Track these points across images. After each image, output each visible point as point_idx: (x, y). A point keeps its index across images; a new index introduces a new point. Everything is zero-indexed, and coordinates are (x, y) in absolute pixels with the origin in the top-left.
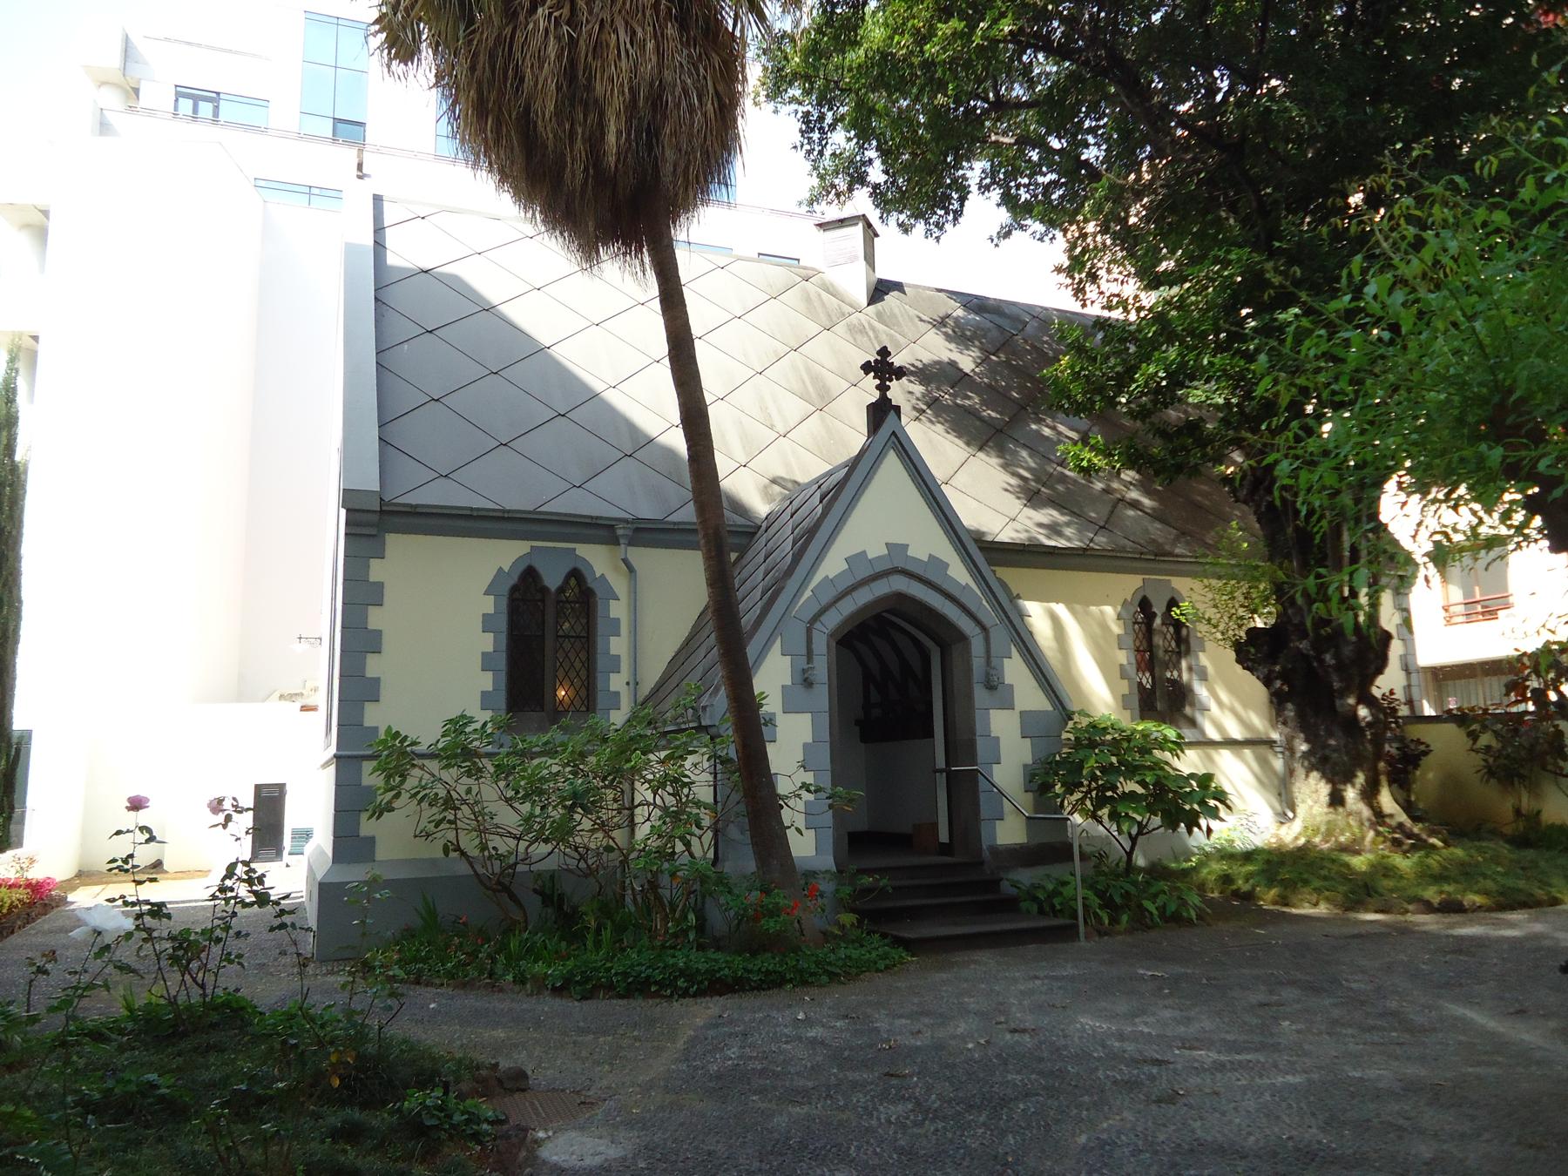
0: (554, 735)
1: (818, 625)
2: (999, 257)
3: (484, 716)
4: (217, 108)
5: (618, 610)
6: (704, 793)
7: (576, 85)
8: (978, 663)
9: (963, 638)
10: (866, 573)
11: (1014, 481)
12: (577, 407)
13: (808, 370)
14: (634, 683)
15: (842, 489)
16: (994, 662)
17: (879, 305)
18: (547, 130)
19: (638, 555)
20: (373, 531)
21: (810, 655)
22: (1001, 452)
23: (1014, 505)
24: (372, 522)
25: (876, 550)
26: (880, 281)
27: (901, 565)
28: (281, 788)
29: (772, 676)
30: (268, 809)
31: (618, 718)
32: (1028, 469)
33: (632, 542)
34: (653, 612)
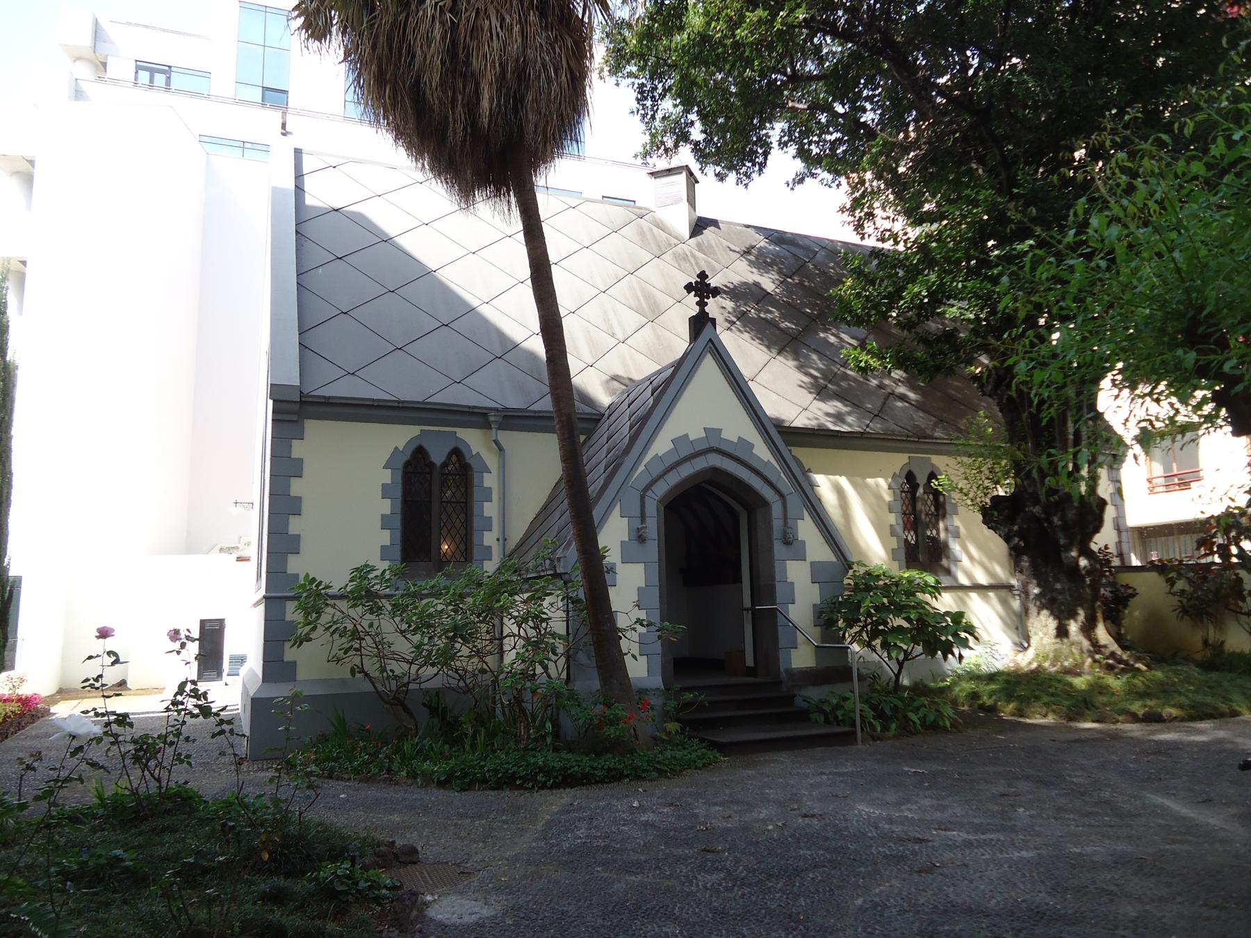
0: (439, 580)
1: (649, 493)
2: (797, 199)
3: (383, 565)
4: (169, 78)
5: (490, 481)
6: (559, 627)
7: (457, 61)
8: (777, 523)
9: (765, 504)
10: (688, 452)
11: (806, 379)
12: (458, 318)
13: (642, 289)
14: (503, 539)
15: (670, 385)
16: (790, 522)
17: (699, 238)
18: (433, 97)
19: (506, 437)
20: (294, 418)
21: (643, 517)
22: (796, 356)
23: (807, 398)
24: (294, 410)
25: (696, 434)
26: (700, 219)
27: (715, 444)
28: (221, 622)
29: (613, 534)
30: (211, 640)
31: (490, 567)
32: (818, 369)
33: (502, 427)
34: (518, 483)
